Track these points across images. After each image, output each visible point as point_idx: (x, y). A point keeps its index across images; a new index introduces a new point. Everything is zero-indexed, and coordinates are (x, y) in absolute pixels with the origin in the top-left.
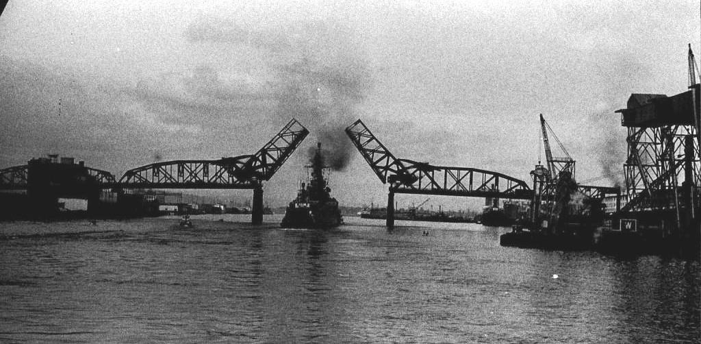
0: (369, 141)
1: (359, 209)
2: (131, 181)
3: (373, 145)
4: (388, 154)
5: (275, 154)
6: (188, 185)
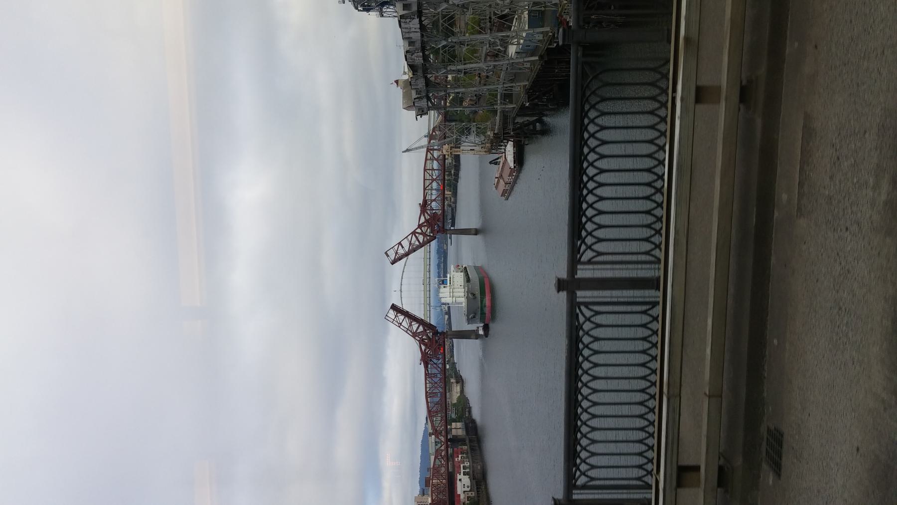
0: (403, 247)
3: (406, 244)
5: (415, 326)
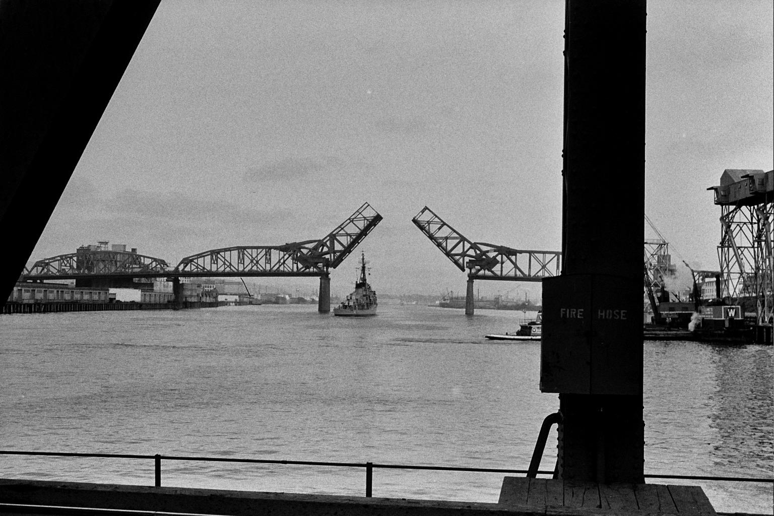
0: (439, 229)
1: (436, 298)
2: (188, 269)
3: (445, 232)
4: (463, 239)
5: (345, 241)
6: (251, 274)
